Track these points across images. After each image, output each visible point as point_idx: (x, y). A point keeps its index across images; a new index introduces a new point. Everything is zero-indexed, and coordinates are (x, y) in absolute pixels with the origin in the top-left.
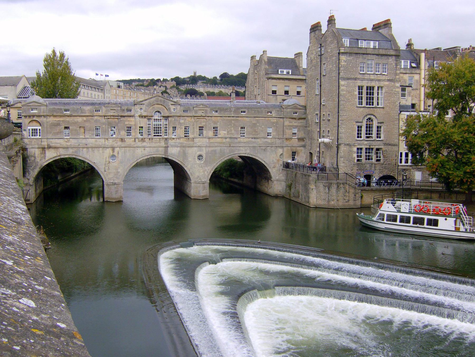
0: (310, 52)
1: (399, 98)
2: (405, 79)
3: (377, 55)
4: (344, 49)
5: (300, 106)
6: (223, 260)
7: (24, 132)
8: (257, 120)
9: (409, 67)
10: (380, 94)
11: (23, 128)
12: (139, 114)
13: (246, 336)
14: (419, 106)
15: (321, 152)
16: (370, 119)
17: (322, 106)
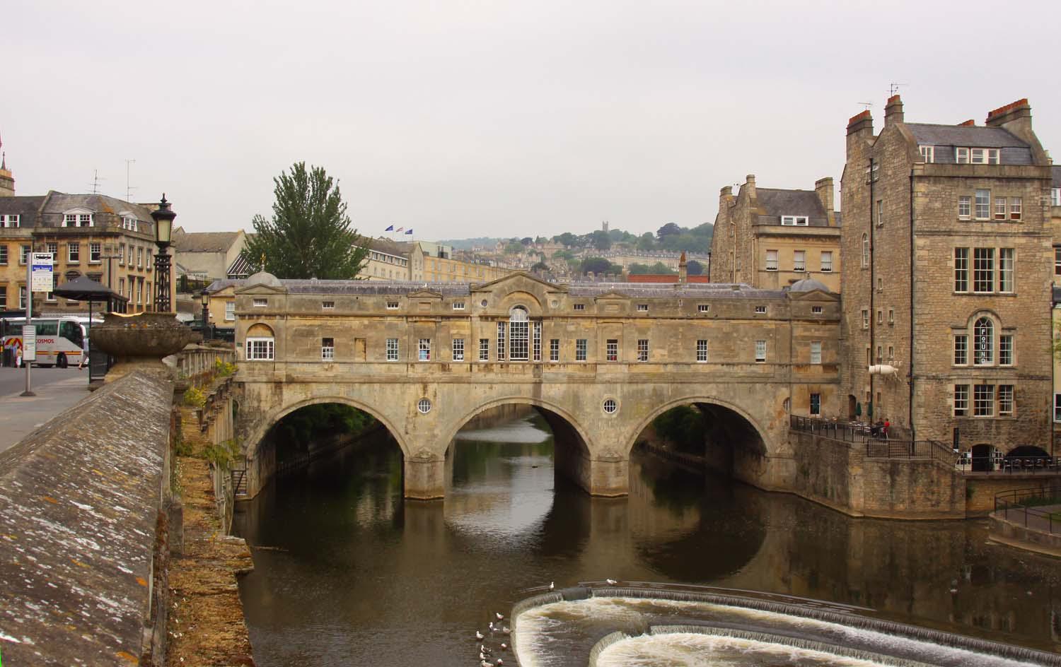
0: (847, 177)
3: (999, 179)
4: (922, 167)
5: (827, 293)
6: (654, 628)
7: (238, 349)
8: (734, 325)
10: (1006, 264)
11: (236, 342)
12: (481, 312)
15: (875, 394)
16: (983, 320)
17: (875, 293)
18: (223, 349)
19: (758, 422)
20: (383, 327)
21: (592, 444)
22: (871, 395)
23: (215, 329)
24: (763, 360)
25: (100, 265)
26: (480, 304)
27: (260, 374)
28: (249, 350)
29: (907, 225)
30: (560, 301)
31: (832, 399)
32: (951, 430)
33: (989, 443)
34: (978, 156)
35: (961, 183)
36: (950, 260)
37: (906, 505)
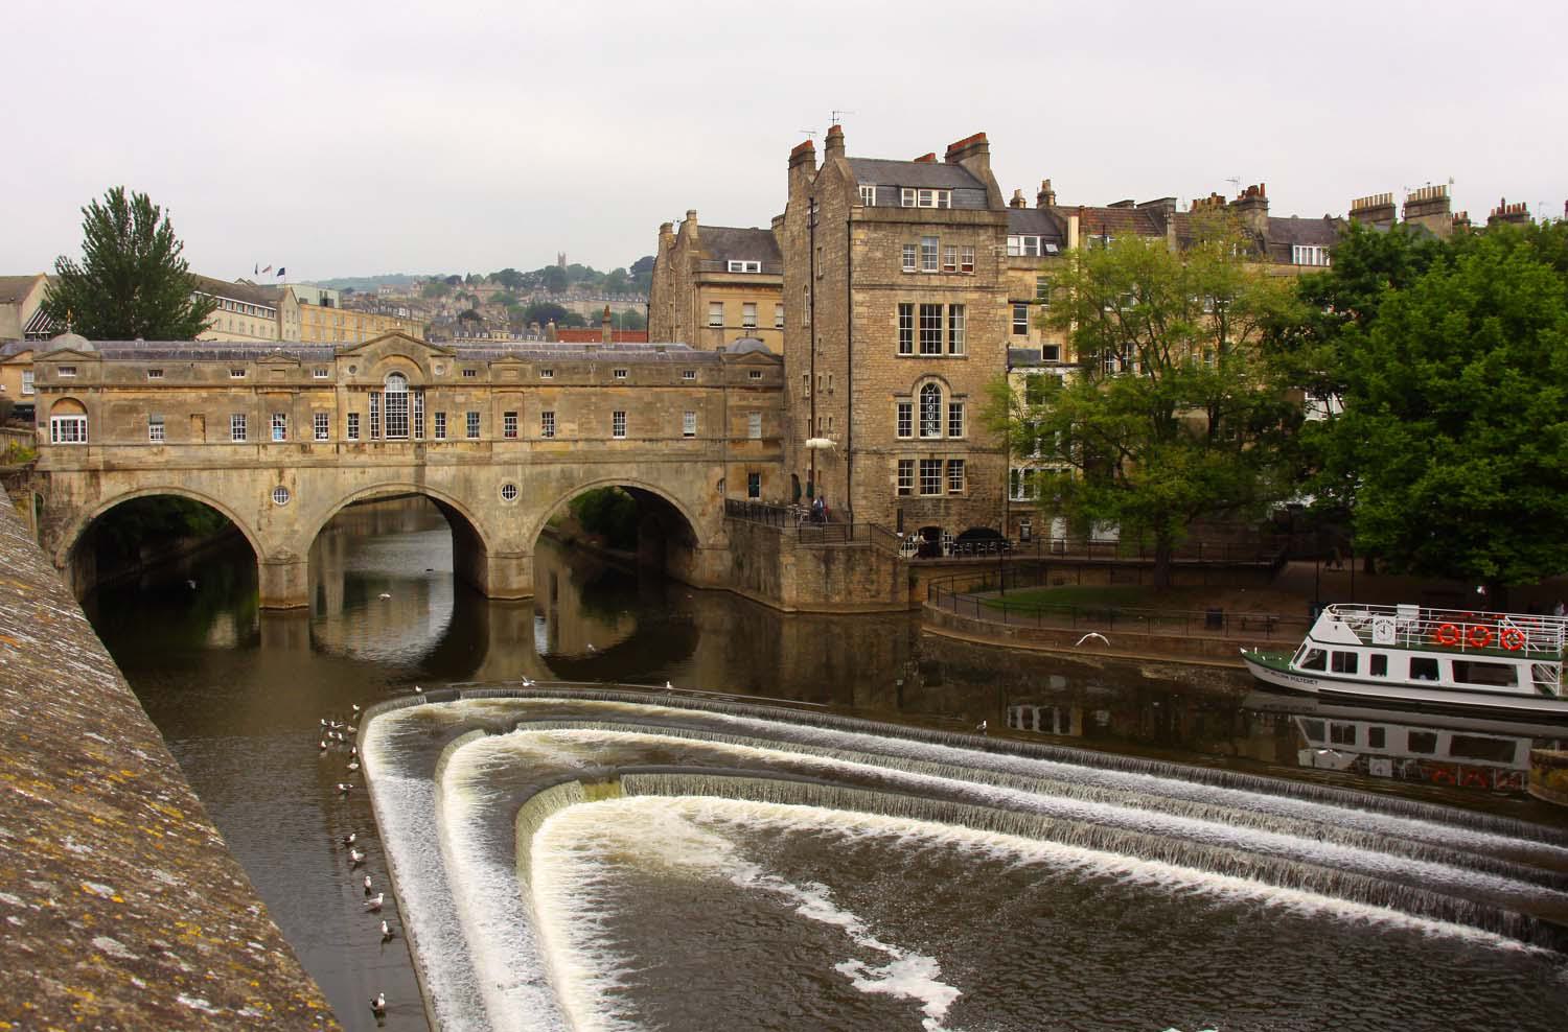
1: (1006, 334)
4: (860, 211)
7: (40, 430)
9: (1039, 254)
11: (37, 420)
13: (526, 909)
16: (930, 386)
18: (20, 430)
20: (226, 400)
21: (489, 538)
26: (347, 371)
27: (69, 462)
28: (55, 430)
29: (845, 278)
31: (773, 479)
32: (895, 511)
34: (926, 199)
37: (843, 597)
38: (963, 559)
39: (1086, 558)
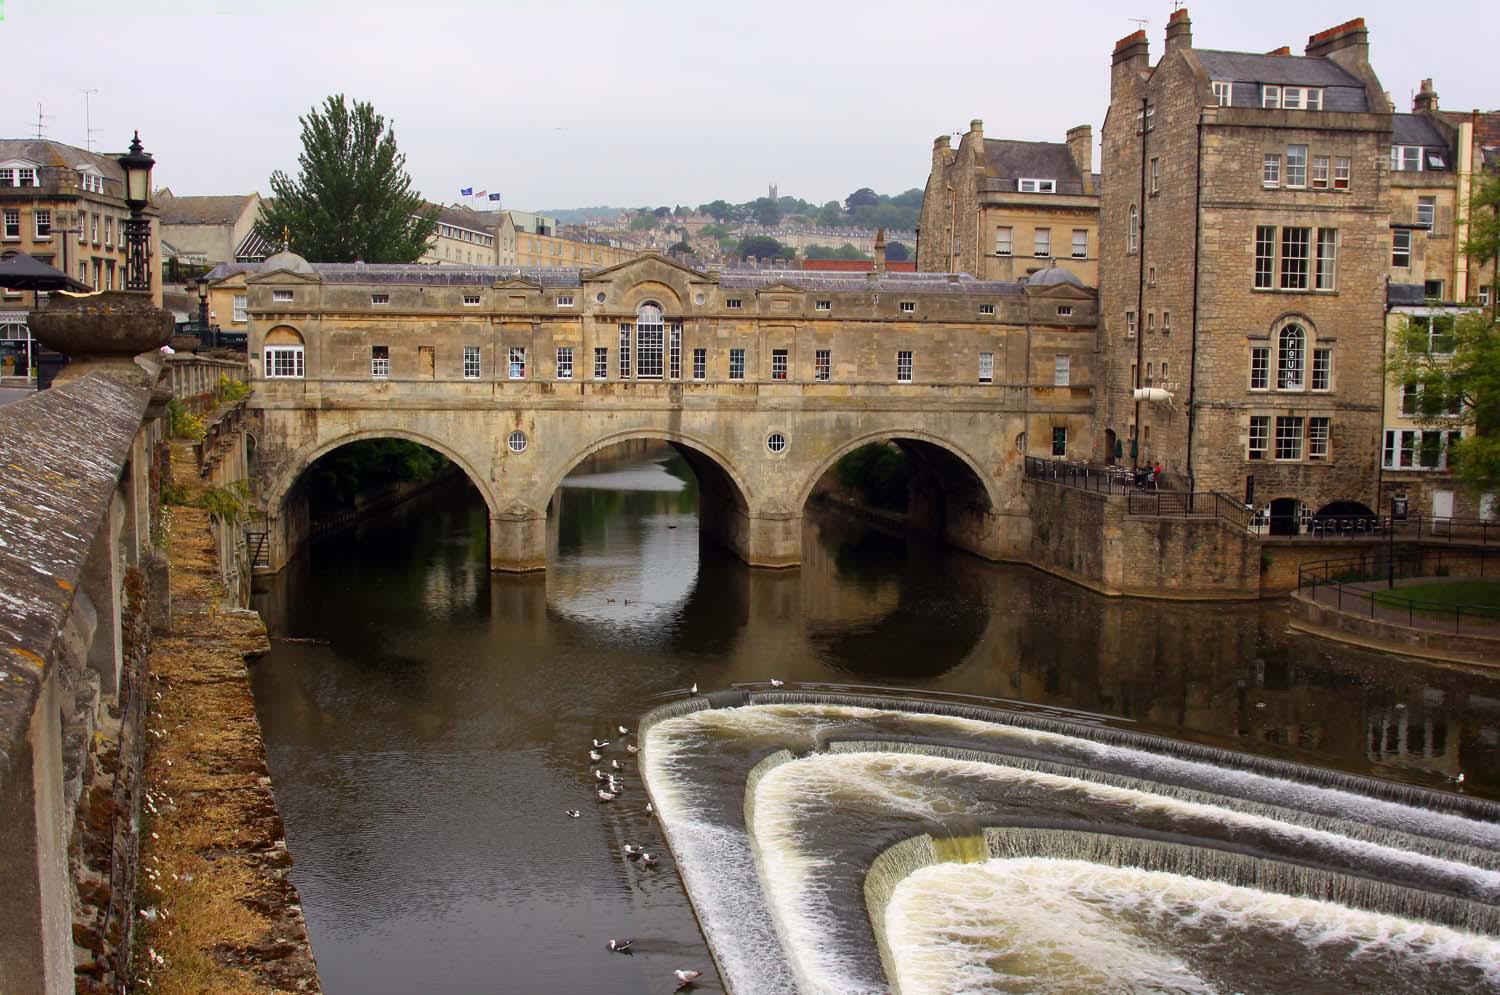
2: (1407, 203)
4: (1214, 112)
7: (253, 362)
9: (1420, 168)
10: (1325, 251)
12: (596, 310)
14: (1452, 289)
15: (1142, 429)
16: (1292, 327)
17: (1145, 288)
18: (232, 362)
19: (981, 466)
21: (752, 496)
22: (1135, 429)
23: (220, 334)
24: (989, 380)
25: (50, 242)
27: (285, 398)
28: (269, 363)
30: (708, 295)
31: (1082, 435)
33: (1294, 497)
34: (1292, 98)
35: (1267, 136)
36: (1250, 243)
38: (1327, 539)
39: (1479, 543)
